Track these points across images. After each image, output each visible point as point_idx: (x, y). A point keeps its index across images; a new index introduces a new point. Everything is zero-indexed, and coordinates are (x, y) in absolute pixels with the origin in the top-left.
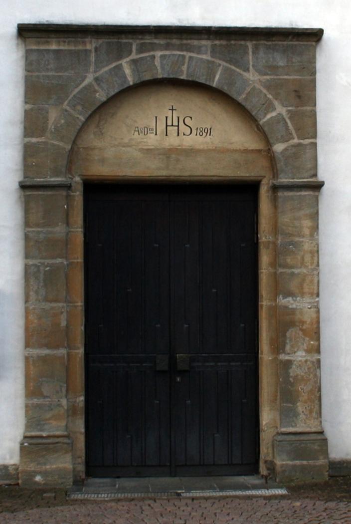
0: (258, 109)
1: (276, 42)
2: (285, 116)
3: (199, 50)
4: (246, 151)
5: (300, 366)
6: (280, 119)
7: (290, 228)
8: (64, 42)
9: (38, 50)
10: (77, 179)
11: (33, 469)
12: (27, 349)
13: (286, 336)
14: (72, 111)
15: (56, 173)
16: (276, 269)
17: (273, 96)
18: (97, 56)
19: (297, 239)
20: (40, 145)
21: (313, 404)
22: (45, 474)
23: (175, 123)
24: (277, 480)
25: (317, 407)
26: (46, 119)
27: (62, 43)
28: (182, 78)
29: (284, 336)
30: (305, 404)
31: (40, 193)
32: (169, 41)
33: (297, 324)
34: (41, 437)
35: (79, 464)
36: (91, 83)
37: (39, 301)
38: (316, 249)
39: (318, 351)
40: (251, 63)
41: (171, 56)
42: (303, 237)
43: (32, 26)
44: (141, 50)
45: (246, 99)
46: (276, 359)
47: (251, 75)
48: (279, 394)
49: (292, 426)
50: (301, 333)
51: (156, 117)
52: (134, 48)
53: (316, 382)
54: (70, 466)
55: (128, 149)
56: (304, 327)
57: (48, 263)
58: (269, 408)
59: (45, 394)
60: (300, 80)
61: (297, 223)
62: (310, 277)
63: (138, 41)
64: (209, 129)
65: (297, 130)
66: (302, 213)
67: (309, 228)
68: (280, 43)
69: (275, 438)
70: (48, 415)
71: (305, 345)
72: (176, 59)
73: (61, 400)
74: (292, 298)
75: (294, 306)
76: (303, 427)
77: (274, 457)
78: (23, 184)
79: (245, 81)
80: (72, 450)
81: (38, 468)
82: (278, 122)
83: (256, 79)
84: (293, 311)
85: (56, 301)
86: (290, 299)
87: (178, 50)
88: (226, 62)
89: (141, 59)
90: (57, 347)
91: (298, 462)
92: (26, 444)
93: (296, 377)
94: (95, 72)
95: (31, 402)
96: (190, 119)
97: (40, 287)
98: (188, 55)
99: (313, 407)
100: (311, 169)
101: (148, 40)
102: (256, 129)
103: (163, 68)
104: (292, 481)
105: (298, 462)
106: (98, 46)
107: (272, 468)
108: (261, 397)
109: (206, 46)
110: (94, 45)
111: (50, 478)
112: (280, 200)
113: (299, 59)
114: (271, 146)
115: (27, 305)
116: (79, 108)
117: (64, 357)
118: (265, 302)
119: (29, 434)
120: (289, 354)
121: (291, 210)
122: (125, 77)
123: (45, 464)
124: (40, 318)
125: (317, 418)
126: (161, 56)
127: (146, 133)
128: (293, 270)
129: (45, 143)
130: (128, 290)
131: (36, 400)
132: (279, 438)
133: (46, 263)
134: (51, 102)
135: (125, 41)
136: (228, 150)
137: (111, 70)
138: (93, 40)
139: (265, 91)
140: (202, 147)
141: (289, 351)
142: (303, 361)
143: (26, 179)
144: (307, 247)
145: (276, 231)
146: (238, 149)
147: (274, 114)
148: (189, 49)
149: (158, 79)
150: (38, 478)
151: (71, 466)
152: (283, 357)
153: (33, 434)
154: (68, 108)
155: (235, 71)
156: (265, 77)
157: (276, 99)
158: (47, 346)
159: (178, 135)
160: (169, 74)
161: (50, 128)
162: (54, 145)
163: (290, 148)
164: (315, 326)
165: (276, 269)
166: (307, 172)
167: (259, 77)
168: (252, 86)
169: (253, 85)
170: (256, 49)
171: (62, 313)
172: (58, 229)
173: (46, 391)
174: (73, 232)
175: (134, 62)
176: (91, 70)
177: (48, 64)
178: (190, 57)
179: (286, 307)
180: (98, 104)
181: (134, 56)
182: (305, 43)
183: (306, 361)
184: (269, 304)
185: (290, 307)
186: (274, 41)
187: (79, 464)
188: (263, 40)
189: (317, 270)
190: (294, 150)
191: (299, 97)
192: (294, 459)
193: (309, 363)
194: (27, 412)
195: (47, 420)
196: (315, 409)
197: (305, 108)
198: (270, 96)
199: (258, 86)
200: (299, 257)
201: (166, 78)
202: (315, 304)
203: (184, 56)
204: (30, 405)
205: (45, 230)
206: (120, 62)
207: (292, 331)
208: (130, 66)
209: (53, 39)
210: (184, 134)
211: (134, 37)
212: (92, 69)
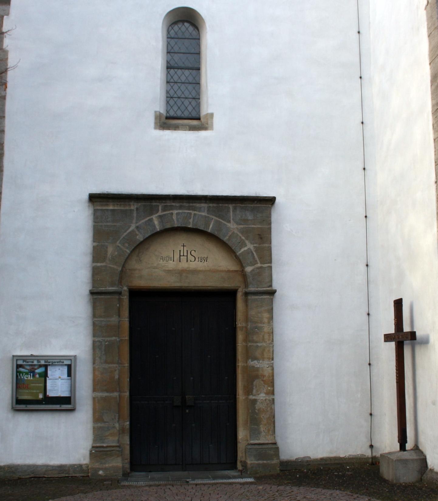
0: (236, 245)
1: (248, 205)
2: (252, 250)
3: (200, 209)
4: (229, 271)
6: (249, 252)
10: (125, 288)
11: (97, 467)
12: (95, 393)
14: (122, 247)
15: (112, 285)
19: (260, 325)
22: (104, 469)
23: (185, 254)
24: (248, 473)
25: (272, 428)
28: (189, 226)
29: (252, 384)
32: (181, 204)
34: (103, 447)
35: (126, 463)
38: (271, 331)
40: (232, 218)
44: (164, 209)
46: (247, 398)
48: (249, 419)
50: (262, 382)
51: (174, 251)
52: (160, 208)
53: (271, 413)
55: (157, 270)
56: (264, 379)
59: (105, 420)
63: (163, 204)
65: (260, 258)
66: (263, 309)
68: (250, 205)
70: (107, 433)
71: (265, 390)
73: (115, 424)
74: (257, 361)
75: (258, 366)
78: (92, 291)
84: (257, 369)
86: (256, 362)
87: (187, 210)
89: (165, 215)
90: (113, 391)
91: (261, 462)
92: (93, 451)
93: (259, 410)
94: (136, 223)
95: (96, 425)
97: (102, 355)
98: (193, 212)
99: (270, 428)
101: (169, 203)
102: (235, 258)
103: (178, 220)
105: (261, 462)
110: (136, 207)
114: (244, 268)
115: (94, 366)
116: (127, 245)
119: (95, 445)
120: (255, 395)
126: (177, 214)
127: (167, 260)
129: (106, 266)
132: (249, 447)
137: (146, 222)
138: (135, 204)
139: (240, 235)
140: (201, 269)
144: (266, 329)
146: (224, 270)
147: (246, 249)
148: (194, 209)
150: (101, 472)
152: (251, 397)
153: (98, 445)
154: (120, 245)
155: (222, 223)
158: (107, 391)
159: (187, 261)
164: (271, 378)
170: (235, 209)
171: (116, 370)
172: (113, 319)
175: (160, 217)
178: (195, 214)
179: (253, 367)
180: (138, 243)
181: (160, 213)
182: (265, 205)
183: (266, 400)
184: (243, 364)
185: (256, 366)
186: (246, 204)
187: (126, 463)
188: (239, 203)
191: (261, 238)
192: (258, 460)
193: (267, 401)
197: (264, 245)
198: (243, 238)
199: (236, 231)
202: (271, 365)
203: (190, 214)
206: (151, 217)
211: (160, 201)
212: (134, 221)
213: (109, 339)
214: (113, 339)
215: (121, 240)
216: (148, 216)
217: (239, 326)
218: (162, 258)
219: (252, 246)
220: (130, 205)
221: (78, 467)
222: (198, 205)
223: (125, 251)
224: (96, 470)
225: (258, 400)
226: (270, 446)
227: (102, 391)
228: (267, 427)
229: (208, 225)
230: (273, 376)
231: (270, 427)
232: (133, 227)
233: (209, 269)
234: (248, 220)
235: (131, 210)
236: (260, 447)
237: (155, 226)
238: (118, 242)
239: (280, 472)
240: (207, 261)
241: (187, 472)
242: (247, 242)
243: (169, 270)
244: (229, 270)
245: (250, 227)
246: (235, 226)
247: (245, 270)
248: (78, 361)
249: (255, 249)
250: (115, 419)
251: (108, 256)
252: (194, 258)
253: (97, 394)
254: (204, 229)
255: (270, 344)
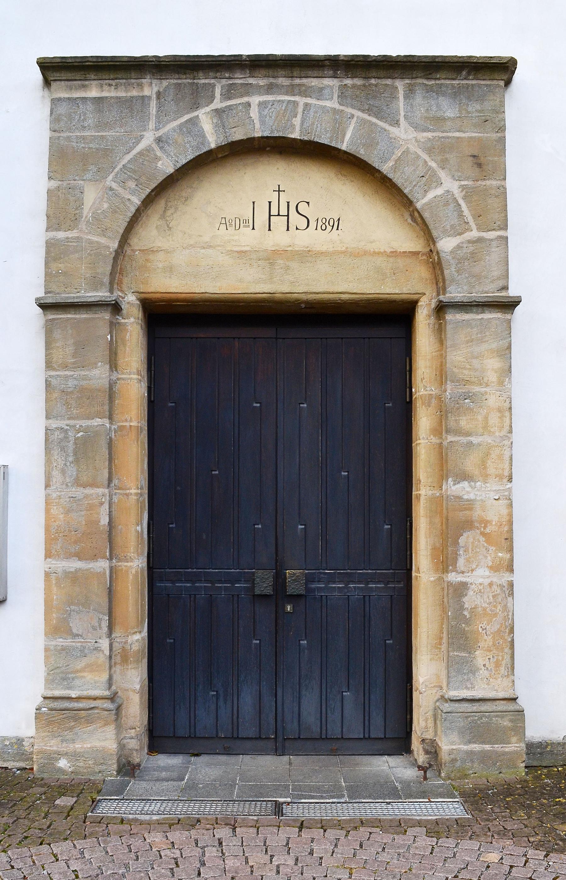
0: (414, 183)
1: (443, 81)
2: (457, 196)
3: (319, 93)
4: (394, 254)
5: (480, 592)
6: (448, 196)
7: (465, 372)
8: (110, 85)
9: (69, 99)
10: (132, 298)
11: (55, 748)
12: (49, 560)
13: (458, 543)
14: (120, 190)
15: (95, 284)
16: (441, 438)
17: (438, 164)
18: (160, 107)
19: (476, 389)
20: (71, 242)
21: (501, 654)
22: (74, 756)
23: (283, 211)
24: (443, 775)
25: (507, 657)
26: (80, 205)
27: (106, 87)
28: (293, 136)
29: (456, 543)
30: (488, 654)
31: (69, 316)
32: (272, 80)
33: (477, 524)
34: (69, 698)
35: (132, 738)
36: (150, 146)
37: (67, 485)
38: (507, 405)
39: (510, 568)
40: (402, 113)
41: (276, 103)
42: (487, 385)
43: (59, 60)
44: (228, 94)
45: (395, 168)
46: (440, 579)
47: (403, 132)
48: (445, 635)
49: (467, 688)
50: (482, 539)
51: (254, 203)
52: (218, 91)
53: (506, 618)
54: (112, 746)
55: (210, 251)
56: (488, 530)
57: (81, 426)
58: (429, 657)
59: (75, 631)
60: (479, 139)
61: (476, 363)
62: (497, 451)
63: (224, 82)
64: (335, 221)
65: (477, 216)
66: (484, 347)
67: (496, 372)
68: (448, 82)
69: (438, 704)
70: (80, 664)
71: (489, 558)
72: (283, 108)
73: (100, 641)
74: (469, 483)
75: (472, 496)
76: (484, 689)
77: (436, 732)
78: (42, 302)
79: (393, 142)
80: (116, 720)
81: (63, 748)
82: (447, 204)
83: (410, 137)
84: (469, 505)
85: (93, 485)
86: (465, 484)
87: (287, 94)
88: (363, 111)
89: (230, 108)
90: (94, 558)
91: (476, 747)
92: (44, 709)
93: (473, 610)
94: (157, 129)
95: (54, 643)
96: (306, 204)
97: (68, 464)
98: (302, 101)
99: (500, 658)
100: (499, 278)
101: (240, 79)
102: (409, 220)
103: (263, 122)
104: (466, 776)
105: (476, 747)
106: (161, 90)
107: (433, 750)
108: (416, 637)
109: (331, 87)
110: (155, 89)
111: (82, 764)
112: (449, 327)
113: (478, 107)
114: (434, 243)
115: (48, 491)
116: (132, 184)
117: (105, 574)
118: (424, 490)
119: (49, 694)
120: (463, 572)
121: (468, 342)
122: (204, 136)
123: (73, 741)
124: (68, 511)
125: (508, 676)
126: (260, 104)
127: (237, 227)
128: (470, 438)
129: (78, 239)
130: (213, 473)
131: (61, 640)
132: (447, 707)
133: (78, 426)
134: (88, 176)
135: (203, 81)
136: (366, 253)
137: (181, 126)
138: (155, 82)
139: (425, 156)
140: (324, 249)
141: (462, 569)
142: (486, 584)
143: (49, 295)
144: (493, 401)
145: (442, 377)
146: (382, 250)
147: (439, 191)
148: (305, 92)
149: (253, 139)
150: (63, 763)
151: (115, 746)
152: (453, 577)
153: (57, 693)
154: (114, 185)
155: (376, 125)
156: (425, 134)
157: (443, 169)
158: (79, 556)
159: (288, 230)
160: (272, 132)
161: (86, 217)
162: (90, 242)
163: (465, 245)
164: (506, 529)
165: (441, 438)
166: (492, 282)
167: (415, 134)
168: (404, 149)
169: (406, 147)
170: (410, 91)
171: (102, 504)
172: (96, 372)
173: (76, 625)
174: (123, 379)
175: (218, 112)
176: (150, 127)
177: (85, 120)
178: (306, 105)
179: (459, 498)
180: (161, 178)
181: (218, 104)
182: (488, 82)
183: (491, 585)
184: (430, 493)
185: (465, 497)
186: (439, 79)
187: (132, 738)
188: (421, 77)
189: (509, 438)
190: (471, 248)
191: (480, 165)
192: (470, 742)
193: (495, 587)
194: (47, 657)
195: (77, 671)
196: (504, 663)
197: (488, 183)
198: (433, 164)
199: (413, 148)
200: (480, 418)
201: (267, 137)
202: (506, 493)
203: (295, 103)
204: (52, 648)
205: (76, 374)
206: (195, 114)
207: (468, 537)
208: (211, 118)
209: (92, 82)
210: (297, 229)
211: (218, 74)
212: (152, 125)
213: (85, 423)
214: (96, 424)
215: (118, 172)
216: (188, 113)
217: (421, 393)
218: (223, 221)
219: (457, 183)
220: (141, 86)
221: (11, 744)
222: (314, 82)
223: (129, 200)
224: (52, 757)
225: (471, 584)
226: (502, 706)
227: (69, 556)
228: (493, 657)
229: (340, 131)
230: (510, 523)
231: (503, 656)
232: (148, 139)
233: (344, 249)
234: (444, 119)
235: (144, 99)
236: (476, 707)
237: (203, 135)
238: (111, 177)
239: (527, 774)
240: (337, 229)
241: (285, 758)
242: (442, 174)
243: (242, 252)
244: (396, 252)
245: (448, 137)
246: (412, 134)
247: (439, 248)
248: (12, 479)
249: (464, 193)
250: (100, 628)
251: (85, 212)
252: (306, 220)
253: (55, 564)
254: (331, 141)
255: (503, 438)
